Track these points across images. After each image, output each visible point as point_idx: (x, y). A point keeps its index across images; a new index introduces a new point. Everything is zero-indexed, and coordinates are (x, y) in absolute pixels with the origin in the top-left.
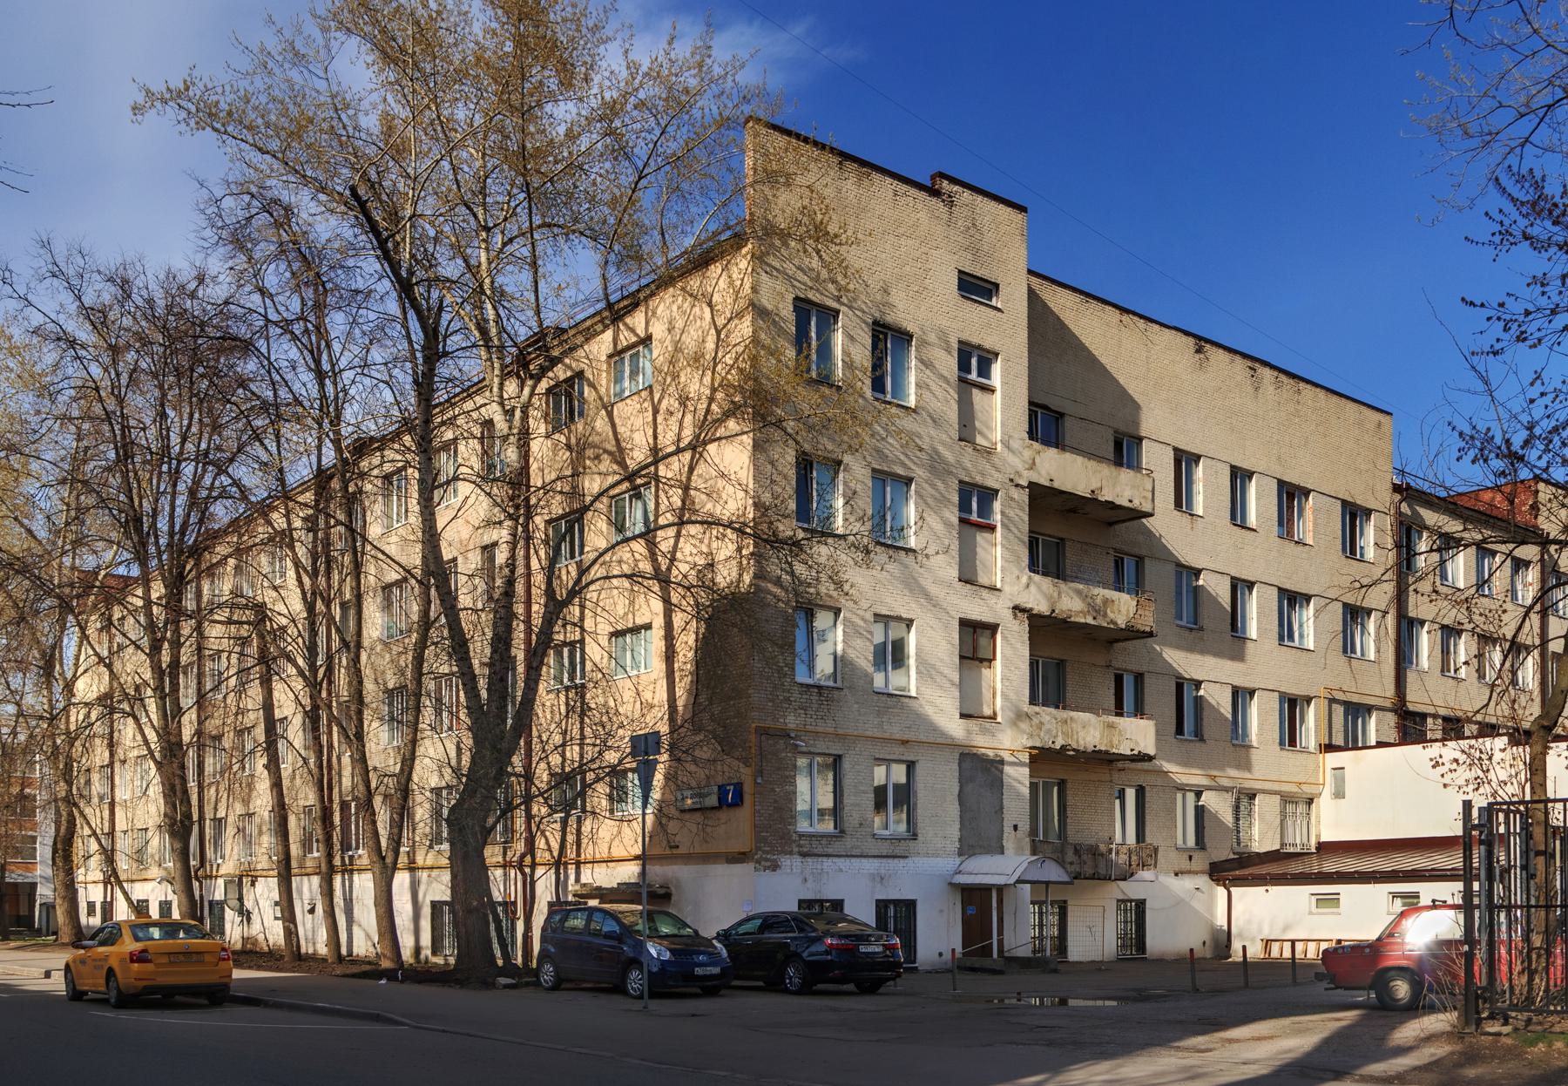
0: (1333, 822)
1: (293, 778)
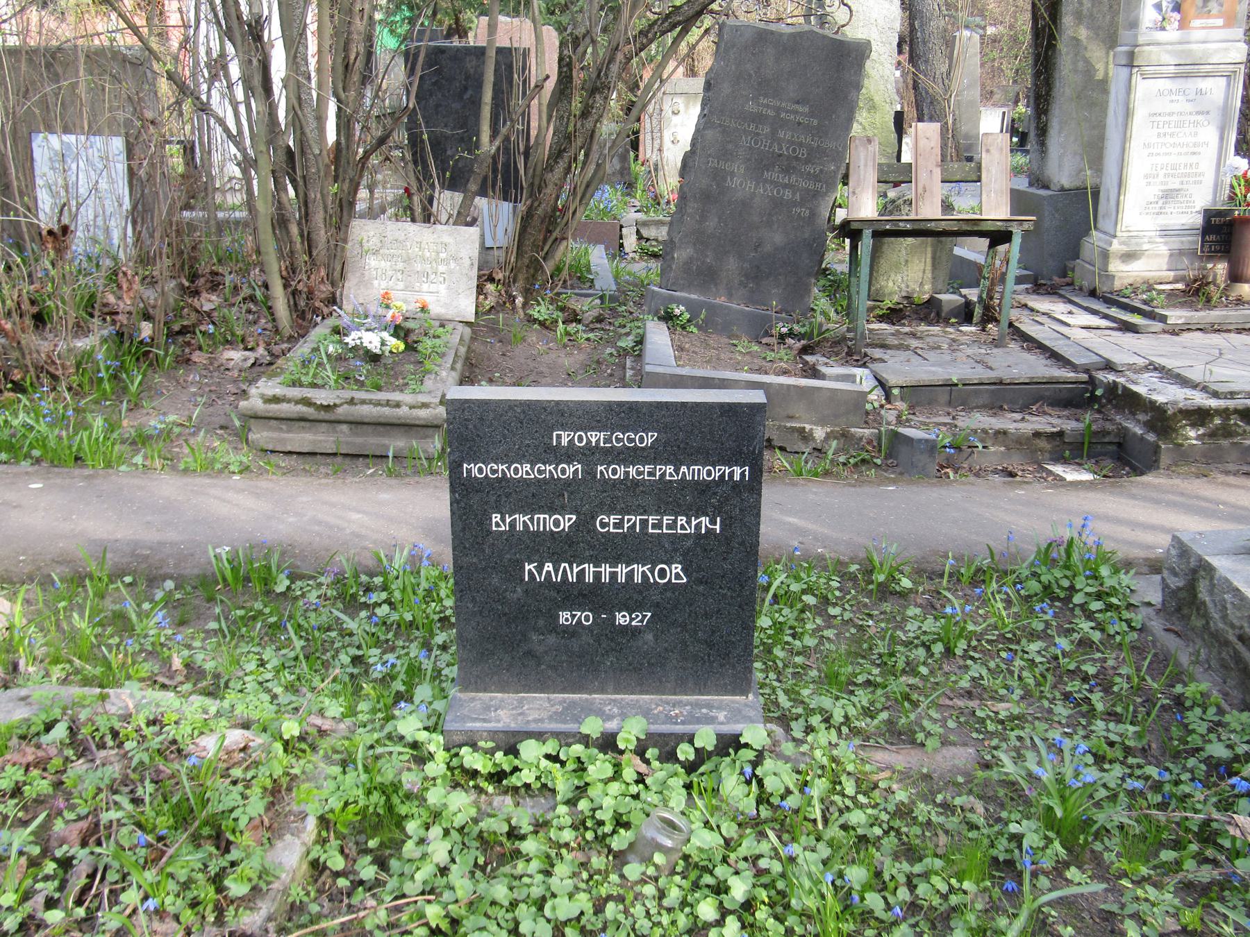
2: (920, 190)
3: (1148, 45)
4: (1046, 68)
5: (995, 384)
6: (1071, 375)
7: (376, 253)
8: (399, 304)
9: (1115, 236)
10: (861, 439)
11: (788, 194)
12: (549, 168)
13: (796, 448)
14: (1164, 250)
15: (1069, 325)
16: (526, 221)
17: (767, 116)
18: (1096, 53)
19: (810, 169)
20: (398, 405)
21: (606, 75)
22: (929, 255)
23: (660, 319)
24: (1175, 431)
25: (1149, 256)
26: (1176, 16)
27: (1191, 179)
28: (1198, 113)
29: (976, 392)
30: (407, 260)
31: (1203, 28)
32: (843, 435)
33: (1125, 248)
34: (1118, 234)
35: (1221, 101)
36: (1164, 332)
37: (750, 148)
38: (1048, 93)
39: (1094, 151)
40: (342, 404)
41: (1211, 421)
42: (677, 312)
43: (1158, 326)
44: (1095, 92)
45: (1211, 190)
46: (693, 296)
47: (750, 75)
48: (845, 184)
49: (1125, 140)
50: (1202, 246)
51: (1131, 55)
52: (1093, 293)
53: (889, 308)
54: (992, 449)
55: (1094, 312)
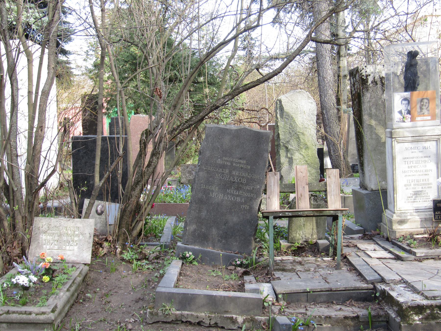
0: (94, 8)
1: (51, 100)
2: (299, 196)
3: (398, 128)
4: (360, 137)
5: (328, 291)
6: (365, 285)
7: (45, 232)
8: (49, 258)
9: (394, 213)
10: (261, 322)
11: (238, 199)
12: (133, 189)
13: (229, 327)
14: (417, 218)
15: (371, 257)
16: (123, 212)
17: (227, 165)
18: (380, 131)
19: (248, 188)
20: (30, 313)
21: (158, 148)
22: (314, 222)
23: (179, 259)
24: (408, 317)
25: (411, 222)
26: (409, 116)
27: (427, 186)
28: (425, 157)
29: (320, 295)
30: (60, 235)
31: (422, 121)
32: (252, 320)
33: (399, 218)
34: (396, 212)
35: (435, 152)
36: (415, 260)
37: (220, 179)
38: (362, 147)
39: (383, 174)
40: (3, 314)
41: (425, 311)
42: (188, 255)
43: (413, 257)
44: (381, 148)
45: (436, 191)
46: (197, 247)
47: (218, 148)
48: (265, 194)
49: (393, 170)
50: (435, 217)
51: (391, 133)
52: (387, 239)
53: (298, 247)
54: (324, 325)
55: (386, 249)
